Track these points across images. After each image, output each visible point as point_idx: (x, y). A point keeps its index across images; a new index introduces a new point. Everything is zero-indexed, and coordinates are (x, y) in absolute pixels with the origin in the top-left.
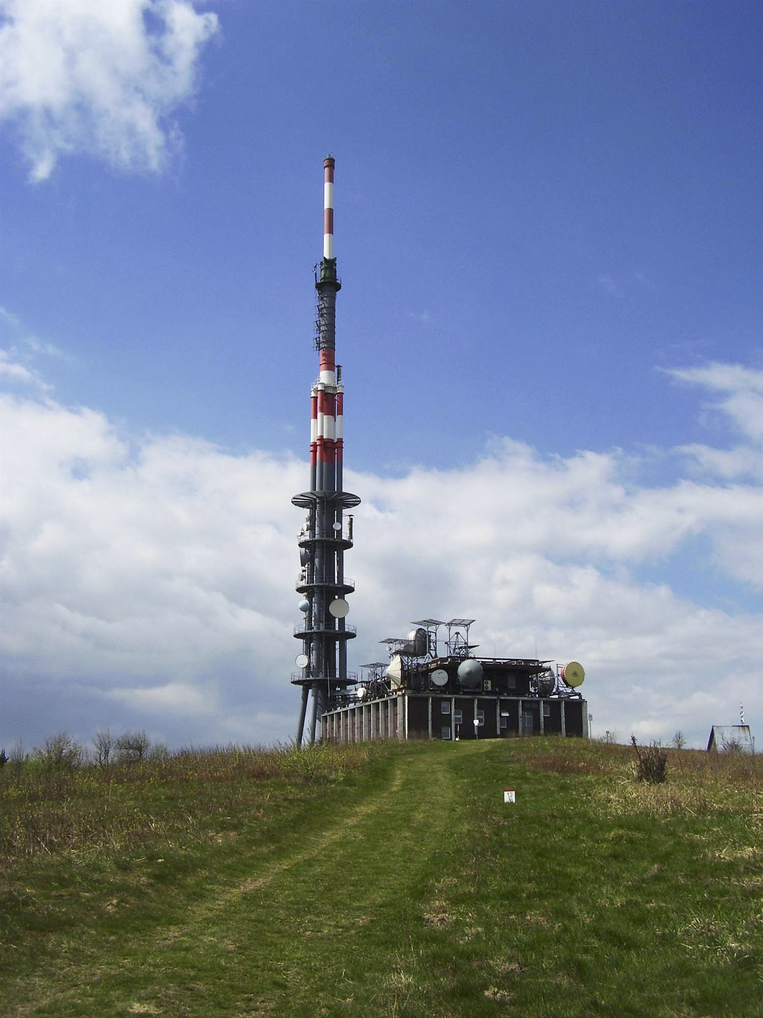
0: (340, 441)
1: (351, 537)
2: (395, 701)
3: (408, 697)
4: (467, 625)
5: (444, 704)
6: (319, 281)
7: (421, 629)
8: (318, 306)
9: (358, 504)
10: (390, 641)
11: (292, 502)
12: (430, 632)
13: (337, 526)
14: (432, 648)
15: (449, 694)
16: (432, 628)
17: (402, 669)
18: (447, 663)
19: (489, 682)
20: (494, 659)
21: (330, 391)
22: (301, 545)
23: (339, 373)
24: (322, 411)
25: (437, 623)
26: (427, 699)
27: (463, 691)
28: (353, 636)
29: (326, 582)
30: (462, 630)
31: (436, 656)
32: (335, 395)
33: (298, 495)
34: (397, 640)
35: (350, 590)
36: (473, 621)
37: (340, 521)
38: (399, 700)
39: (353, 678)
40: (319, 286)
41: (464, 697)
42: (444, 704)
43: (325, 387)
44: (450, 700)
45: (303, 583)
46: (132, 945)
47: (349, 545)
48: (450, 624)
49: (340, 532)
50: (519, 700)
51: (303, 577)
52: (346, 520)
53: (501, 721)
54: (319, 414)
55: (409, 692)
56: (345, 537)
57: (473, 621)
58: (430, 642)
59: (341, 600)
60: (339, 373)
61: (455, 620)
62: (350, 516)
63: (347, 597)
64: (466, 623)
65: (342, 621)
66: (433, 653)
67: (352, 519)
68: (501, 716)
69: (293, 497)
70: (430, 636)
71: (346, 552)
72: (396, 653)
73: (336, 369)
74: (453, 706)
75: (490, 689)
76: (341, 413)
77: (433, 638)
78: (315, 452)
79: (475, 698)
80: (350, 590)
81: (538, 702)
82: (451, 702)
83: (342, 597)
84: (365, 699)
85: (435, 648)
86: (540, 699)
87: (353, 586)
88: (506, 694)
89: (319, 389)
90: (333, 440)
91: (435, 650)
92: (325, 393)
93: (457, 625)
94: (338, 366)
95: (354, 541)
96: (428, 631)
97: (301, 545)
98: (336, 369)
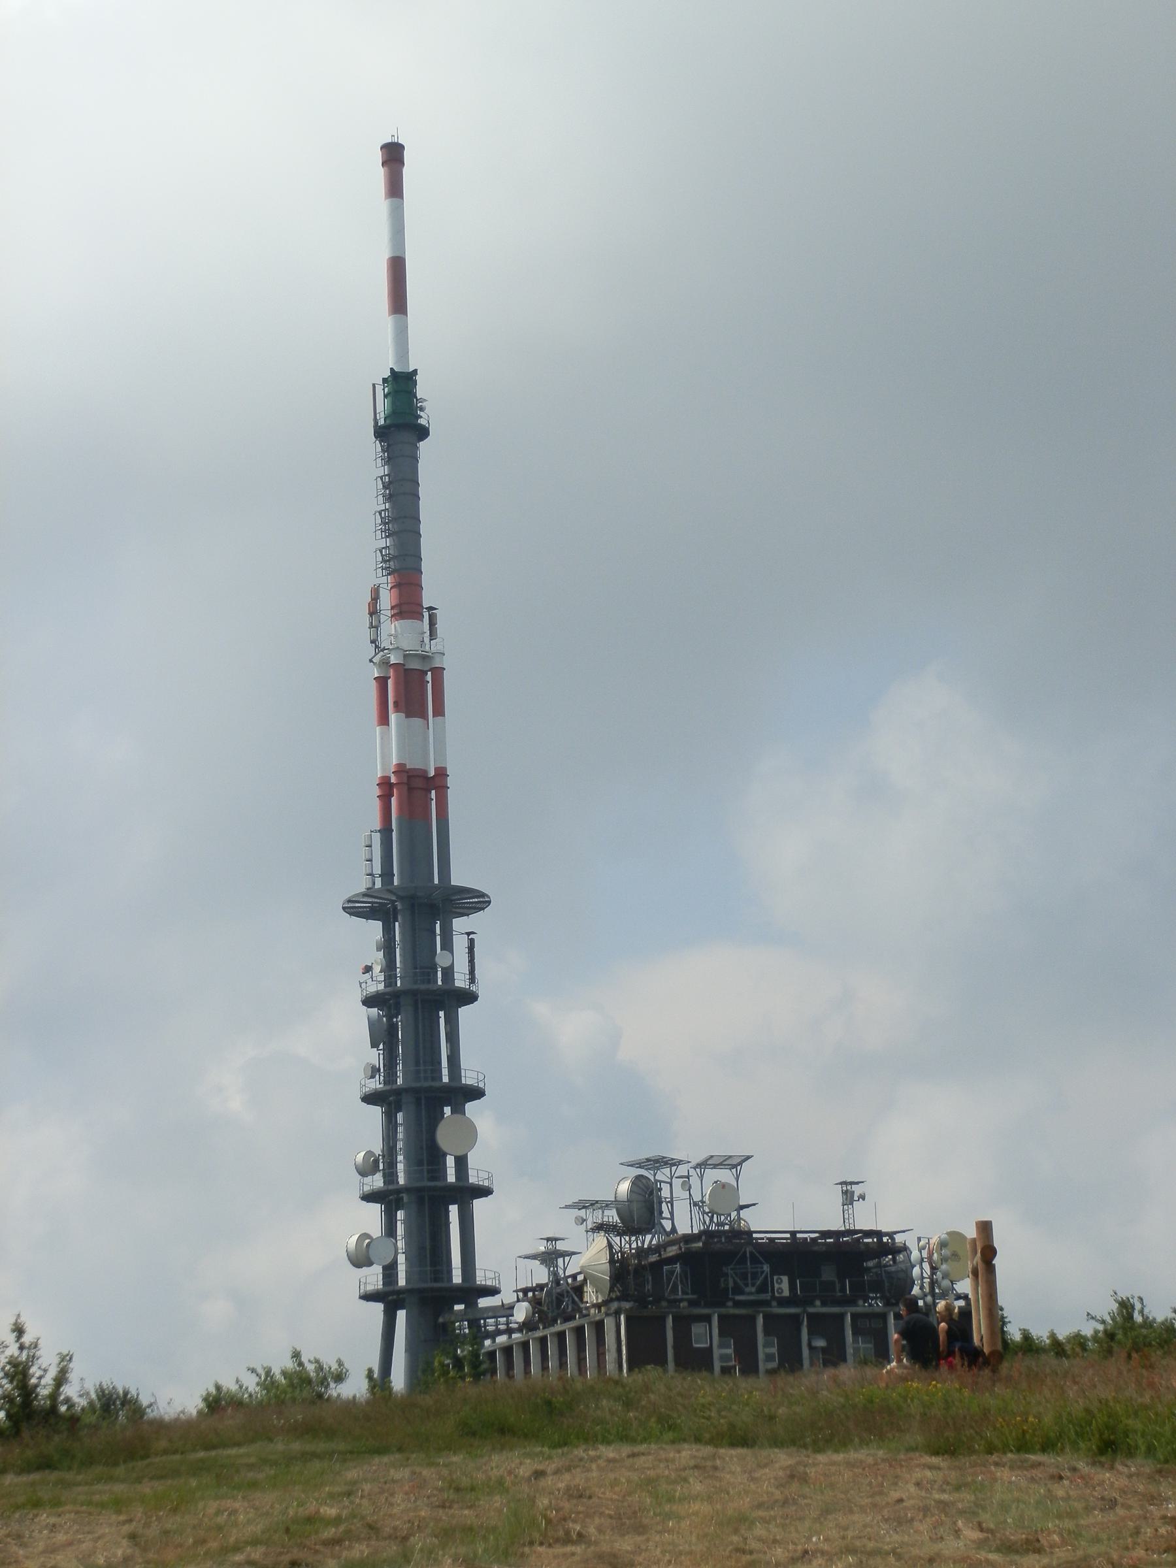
0: (442, 773)
1: (472, 980)
2: (599, 1326)
3: (628, 1319)
4: (735, 1166)
5: (697, 1329)
6: (381, 422)
7: (642, 1176)
8: (381, 478)
9: (483, 909)
10: (583, 1205)
11: (344, 908)
12: (661, 1182)
13: (442, 958)
14: (666, 1214)
15: (707, 1305)
16: (663, 1174)
17: (612, 1261)
18: (700, 1244)
19: (785, 1279)
20: (793, 1233)
21: (414, 665)
22: (369, 1002)
23: (432, 623)
24: (397, 707)
25: (673, 1163)
26: (663, 1319)
27: (733, 1300)
28: (485, 1192)
29: (426, 1079)
30: (725, 1176)
31: (674, 1230)
32: (425, 673)
33: (357, 895)
34: (597, 1202)
35: (476, 1093)
36: (748, 1158)
37: (448, 945)
38: (609, 1323)
39: (489, 1283)
40: (381, 433)
41: (737, 1311)
42: (697, 1329)
43: (405, 656)
44: (707, 1319)
45: (376, 1084)
46: (877, 1437)
47: (469, 997)
48: (702, 1165)
49: (449, 972)
50: (846, 1313)
51: (374, 1071)
52: (460, 944)
53: (811, 1359)
54: (393, 717)
55: (627, 1305)
56: (461, 981)
57: (748, 1158)
58: (660, 1203)
59: (458, 1116)
60: (432, 623)
61: (712, 1157)
62: (468, 934)
63: (470, 1107)
64: (735, 1162)
65: (461, 1162)
66: (668, 1225)
67: (472, 942)
68: (811, 1347)
69: (347, 897)
70: (660, 1189)
71: (464, 1012)
72: (600, 1227)
73: (426, 615)
74: (716, 1331)
75: (786, 1293)
76: (439, 711)
77: (665, 1193)
78: (385, 798)
79: (714, 1313)
80: (476, 1093)
81: (883, 1317)
82: (799, 1324)
83: (459, 1110)
84: (527, 1326)
85: (672, 1213)
86: (886, 1309)
87: (481, 1085)
88: (818, 1303)
89: (393, 661)
90: (425, 772)
91: (672, 1219)
92: (406, 670)
93: (715, 1166)
94: (430, 609)
95: (481, 989)
96: (656, 1181)
97: (369, 1002)
98: (426, 615)
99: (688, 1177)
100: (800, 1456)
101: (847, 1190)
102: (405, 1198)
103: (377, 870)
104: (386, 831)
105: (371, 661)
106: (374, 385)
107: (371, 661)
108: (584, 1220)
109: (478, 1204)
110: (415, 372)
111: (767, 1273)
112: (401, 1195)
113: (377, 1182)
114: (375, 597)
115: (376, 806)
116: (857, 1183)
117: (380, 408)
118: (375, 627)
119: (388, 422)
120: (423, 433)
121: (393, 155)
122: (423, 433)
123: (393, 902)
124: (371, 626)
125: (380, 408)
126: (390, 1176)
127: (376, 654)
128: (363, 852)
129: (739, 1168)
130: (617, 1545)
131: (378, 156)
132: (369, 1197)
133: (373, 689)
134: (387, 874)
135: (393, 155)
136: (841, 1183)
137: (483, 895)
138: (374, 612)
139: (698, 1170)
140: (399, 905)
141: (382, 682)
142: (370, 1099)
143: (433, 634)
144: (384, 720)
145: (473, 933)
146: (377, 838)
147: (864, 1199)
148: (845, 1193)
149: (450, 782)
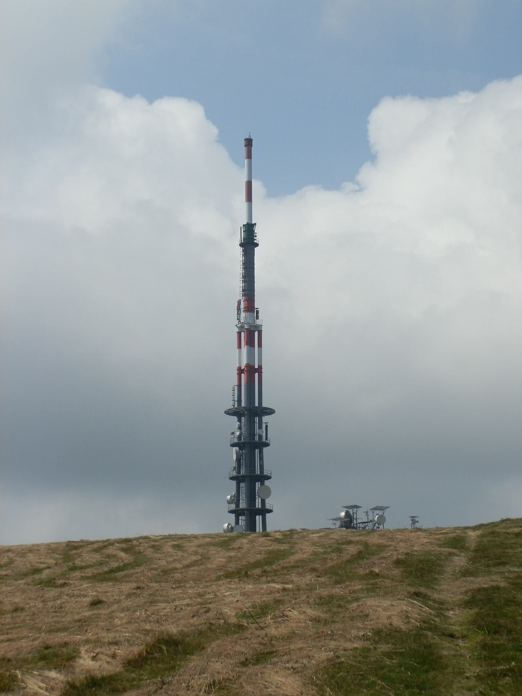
1: (266, 439)
21: (252, 329)
28: (270, 511)
35: (268, 478)
37: (260, 427)
45: (234, 474)
47: (267, 445)
63: (267, 482)
64: (384, 508)
83: (262, 484)
99: (367, 512)
100: (274, 596)
101: (413, 520)
102: (246, 512)
103: (236, 399)
104: (239, 386)
105: (236, 326)
106: (241, 228)
107: (236, 326)
108: (335, 524)
109: (268, 515)
110: (255, 224)
111: (266, 540)
112: (244, 511)
113: (233, 507)
114: (239, 303)
115: (236, 376)
116: (416, 517)
117: (242, 237)
118: (239, 314)
119: (244, 241)
120: (257, 245)
121: (249, 143)
122: (257, 245)
123: (243, 411)
124: (238, 314)
125: (242, 237)
126: (237, 505)
127: (239, 324)
128: (231, 393)
129: (384, 510)
130: (54, 592)
131: (243, 143)
132: (231, 512)
133: (236, 336)
134: (239, 401)
135: (249, 143)
136: (411, 517)
137: (226, 414)
138: (239, 309)
139: (372, 511)
140: (246, 413)
141: (239, 334)
142: (232, 478)
143: (257, 318)
144: (240, 346)
145: (267, 423)
146: (236, 388)
147: (418, 522)
148: (412, 520)
149: (263, 370)
